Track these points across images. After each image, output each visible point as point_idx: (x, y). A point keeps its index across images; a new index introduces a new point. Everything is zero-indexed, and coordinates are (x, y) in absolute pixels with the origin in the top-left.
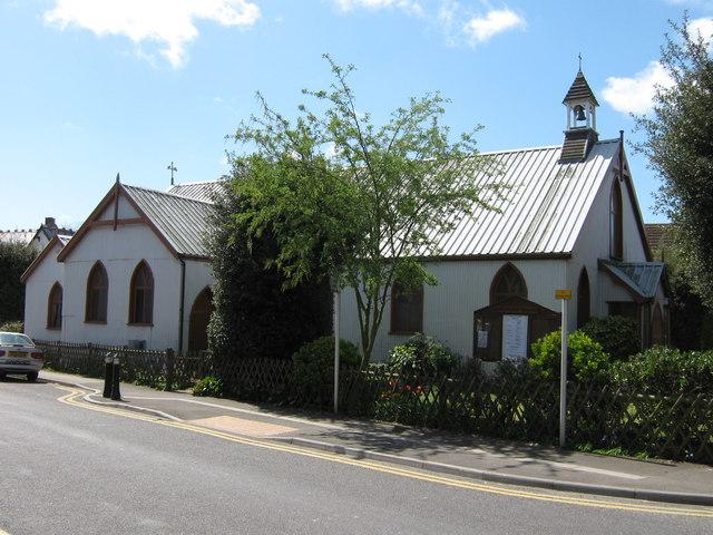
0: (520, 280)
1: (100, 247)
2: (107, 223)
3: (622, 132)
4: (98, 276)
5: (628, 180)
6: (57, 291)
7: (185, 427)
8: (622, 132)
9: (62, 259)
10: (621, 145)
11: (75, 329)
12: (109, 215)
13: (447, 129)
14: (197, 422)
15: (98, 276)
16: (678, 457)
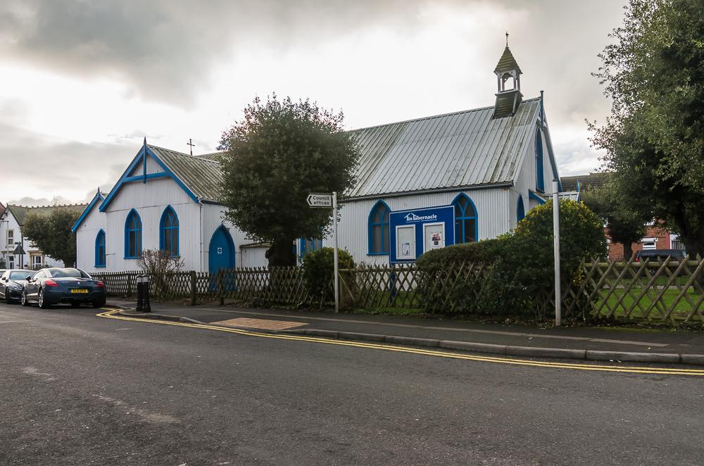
0: (472, 210)
1: (133, 198)
2: (139, 179)
3: (542, 92)
4: (133, 220)
5: (546, 130)
6: (101, 236)
7: (205, 327)
8: (542, 92)
9: (105, 209)
10: (542, 102)
11: (118, 262)
12: (140, 173)
13: (257, 100)
14: (224, 323)
15: (133, 220)
16: (500, 324)
